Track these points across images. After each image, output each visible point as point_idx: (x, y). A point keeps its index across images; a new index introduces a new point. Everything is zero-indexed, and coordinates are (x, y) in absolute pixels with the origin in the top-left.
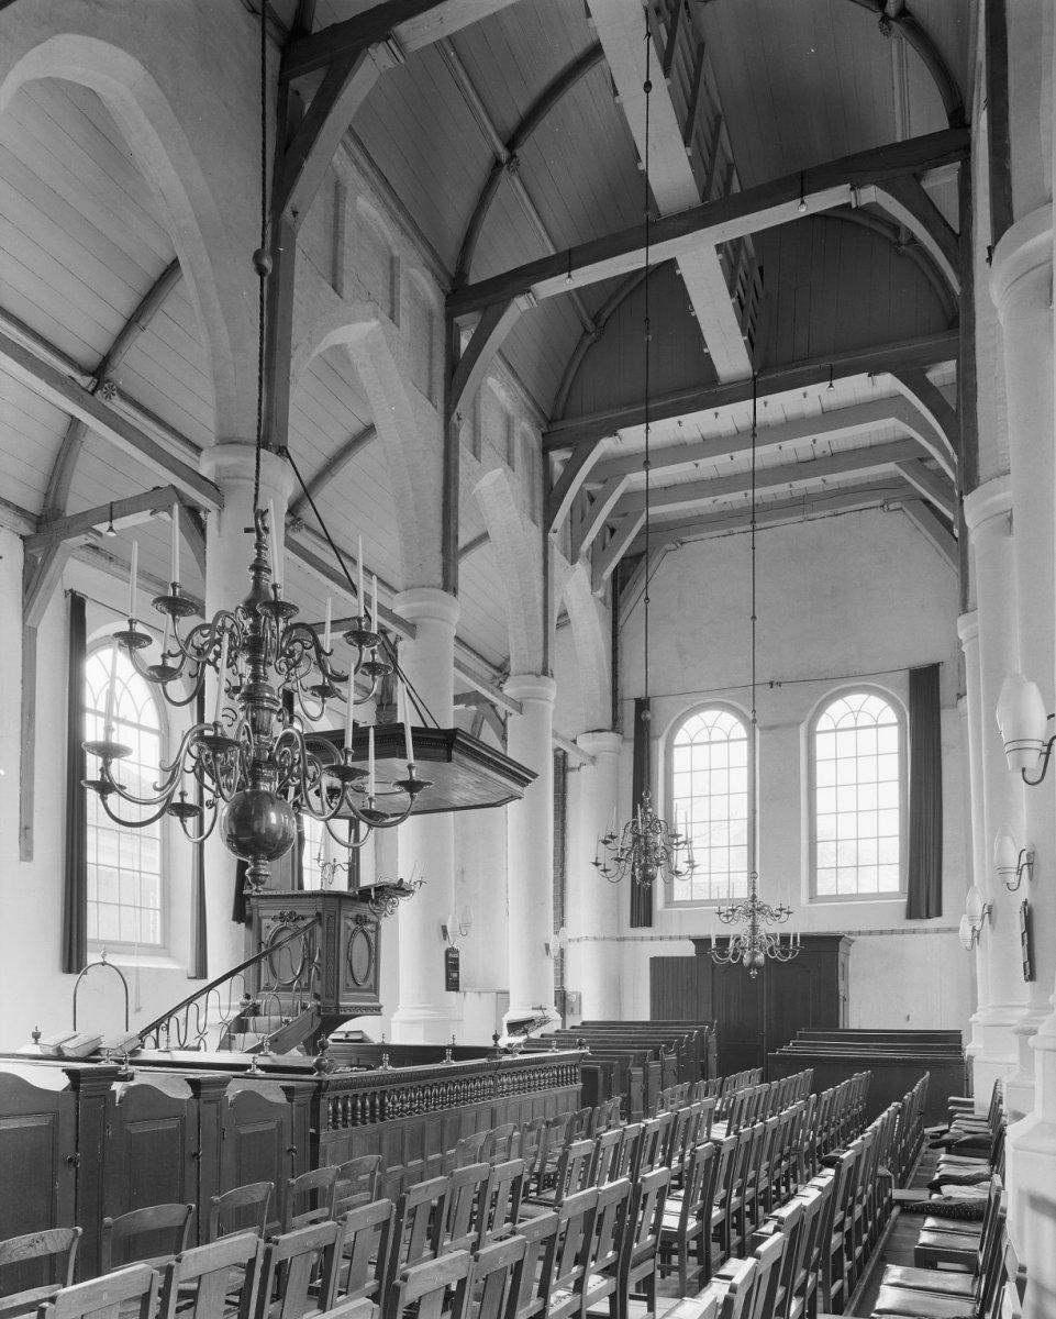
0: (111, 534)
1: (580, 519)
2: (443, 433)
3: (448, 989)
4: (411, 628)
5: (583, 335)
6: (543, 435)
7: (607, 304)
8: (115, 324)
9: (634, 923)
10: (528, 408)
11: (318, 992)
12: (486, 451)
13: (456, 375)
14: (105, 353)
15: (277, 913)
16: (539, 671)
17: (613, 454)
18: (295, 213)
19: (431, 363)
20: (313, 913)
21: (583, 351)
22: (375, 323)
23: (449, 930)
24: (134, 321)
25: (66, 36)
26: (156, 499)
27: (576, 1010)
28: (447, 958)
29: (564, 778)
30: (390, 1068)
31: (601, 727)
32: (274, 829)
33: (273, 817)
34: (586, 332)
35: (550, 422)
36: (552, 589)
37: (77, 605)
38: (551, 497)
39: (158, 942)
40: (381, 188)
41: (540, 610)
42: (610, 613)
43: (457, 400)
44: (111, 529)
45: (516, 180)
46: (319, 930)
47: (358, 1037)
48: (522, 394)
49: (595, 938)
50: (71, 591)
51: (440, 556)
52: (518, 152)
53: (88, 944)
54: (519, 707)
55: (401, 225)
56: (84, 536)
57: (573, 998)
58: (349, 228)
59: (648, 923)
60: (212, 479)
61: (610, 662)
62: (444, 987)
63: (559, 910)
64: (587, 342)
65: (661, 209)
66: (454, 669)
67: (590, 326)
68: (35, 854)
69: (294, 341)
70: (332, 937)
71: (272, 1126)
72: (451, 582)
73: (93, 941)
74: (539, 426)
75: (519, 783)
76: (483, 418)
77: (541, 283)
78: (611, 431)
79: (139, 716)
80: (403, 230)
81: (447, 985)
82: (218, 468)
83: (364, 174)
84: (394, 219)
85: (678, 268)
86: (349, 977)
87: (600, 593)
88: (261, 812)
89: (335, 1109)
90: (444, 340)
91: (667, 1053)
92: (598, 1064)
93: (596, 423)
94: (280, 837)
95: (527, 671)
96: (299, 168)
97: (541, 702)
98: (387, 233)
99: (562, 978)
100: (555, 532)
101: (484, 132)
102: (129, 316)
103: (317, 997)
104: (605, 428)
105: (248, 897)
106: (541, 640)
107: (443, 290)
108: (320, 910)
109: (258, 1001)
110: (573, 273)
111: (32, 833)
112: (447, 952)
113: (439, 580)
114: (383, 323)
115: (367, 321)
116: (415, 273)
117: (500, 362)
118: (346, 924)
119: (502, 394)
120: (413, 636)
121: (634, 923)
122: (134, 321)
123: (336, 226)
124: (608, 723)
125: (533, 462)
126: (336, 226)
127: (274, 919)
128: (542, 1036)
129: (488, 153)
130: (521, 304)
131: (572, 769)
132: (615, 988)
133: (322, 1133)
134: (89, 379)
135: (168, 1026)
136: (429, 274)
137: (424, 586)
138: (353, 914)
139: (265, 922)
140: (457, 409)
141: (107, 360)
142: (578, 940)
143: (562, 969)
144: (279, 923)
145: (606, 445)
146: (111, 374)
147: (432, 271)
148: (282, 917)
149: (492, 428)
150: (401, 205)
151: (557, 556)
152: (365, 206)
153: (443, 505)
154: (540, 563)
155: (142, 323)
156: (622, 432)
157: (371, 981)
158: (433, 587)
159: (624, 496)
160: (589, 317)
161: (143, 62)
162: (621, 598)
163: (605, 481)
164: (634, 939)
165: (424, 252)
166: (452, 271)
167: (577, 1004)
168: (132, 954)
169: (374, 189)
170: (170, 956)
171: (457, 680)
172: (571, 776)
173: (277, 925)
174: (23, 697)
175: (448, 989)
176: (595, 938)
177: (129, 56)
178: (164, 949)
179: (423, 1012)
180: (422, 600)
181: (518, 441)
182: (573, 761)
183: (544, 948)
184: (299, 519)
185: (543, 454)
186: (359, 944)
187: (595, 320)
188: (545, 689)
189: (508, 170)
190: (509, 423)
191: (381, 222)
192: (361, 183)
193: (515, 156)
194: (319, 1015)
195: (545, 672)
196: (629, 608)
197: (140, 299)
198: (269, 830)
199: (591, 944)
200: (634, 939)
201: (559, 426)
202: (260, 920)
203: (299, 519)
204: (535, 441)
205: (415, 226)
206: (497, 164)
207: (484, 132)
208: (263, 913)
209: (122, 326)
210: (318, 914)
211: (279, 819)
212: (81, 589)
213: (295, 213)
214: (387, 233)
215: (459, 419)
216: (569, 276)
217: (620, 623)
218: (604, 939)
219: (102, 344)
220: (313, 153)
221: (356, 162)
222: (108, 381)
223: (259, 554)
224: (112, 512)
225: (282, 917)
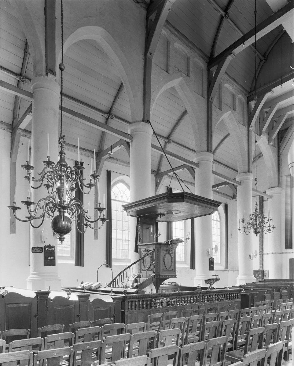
0: (112, 154)
1: (262, 120)
2: (207, 105)
3: (210, 270)
4: (197, 165)
5: (260, 61)
6: (247, 97)
7: (267, 50)
8: (112, 99)
9: (286, 248)
10: (241, 90)
11: (154, 271)
12: (224, 107)
13: (211, 86)
14: (110, 107)
15: (145, 250)
16: (247, 171)
17: (278, 96)
18: (151, 54)
19: (202, 85)
20: (153, 249)
21: (260, 67)
22: (181, 78)
23: (209, 252)
24: (116, 97)
25: (82, 28)
26: (120, 142)
27: (267, 276)
28: (210, 261)
29: (263, 204)
30: (180, 292)
31: (274, 186)
32: (64, 225)
33: (64, 223)
34: (261, 61)
35: (249, 93)
36: (251, 145)
37: (109, 173)
38: (250, 115)
39: (184, 260)
40: (182, 38)
41: (247, 152)
42: (276, 149)
43: (211, 94)
44: (111, 152)
45: (229, 20)
46: (154, 253)
47: (174, 284)
48: (238, 87)
49: (273, 253)
50: (107, 170)
51: (206, 142)
52: (228, 11)
53: (113, 260)
54: (240, 183)
55: (190, 47)
56: (106, 155)
57: (265, 272)
58: (171, 53)
59: (291, 247)
60: (130, 134)
61: (277, 165)
62: (209, 269)
63: (262, 245)
64: (262, 63)
65: (273, 10)
66: (212, 174)
67: (262, 58)
68: (98, 238)
69: (152, 90)
70: (158, 256)
71: (107, 308)
72: (210, 149)
73: (114, 259)
74: (246, 95)
75: (214, 206)
76: (222, 97)
77: (235, 49)
78: (269, 90)
79: (116, 198)
80: (191, 48)
81: (52, 265)
82: (131, 130)
83: (176, 36)
84: (188, 46)
85: (284, 28)
86: (164, 266)
87: (272, 143)
88: (59, 221)
89: (132, 305)
90: (207, 77)
91: (283, 289)
92: (248, 293)
93: (264, 89)
94: (66, 227)
95: (243, 172)
96: (151, 40)
97: (247, 181)
98: (186, 51)
99: (262, 266)
100: (252, 127)
101: (216, 10)
102: (115, 96)
103: (154, 272)
104: (268, 90)
105: (138, 245)
106: (247, 162)
107: (206, 62)
108: (155, 248)
109: (141, 274)
110: (245, 43)
111: (98, 232)
112: (210, 259)
113: (206, 149)
114: (184, 77)
115: (178, 78)
116: (196, 60)
117: (229, 79)
118: (162, 253)
119: (231, 88)
120: (198, 167)
121: (286, 248)
122: (116, 97)
123: (167, 54)
124: (276, 185)
125: (244, 107)
126: (167, 54)
127: (144, 251)
128: (247, 284)
129: (219, 15)
130: (230, 58)
131: (265, 201)
132: (279, 268)
133: (126, 311)
134: (107, 115)
135: (115, 281)
136: (201, 58)
137: (201, 152)
138: (165, 249)
139: (142, 252)
140: (211, 96)
141: (111, 109)
142: (268, 254)
143: (262, 263)
144: (145, 252)
145: (268, 95)
146: (112, 112)
147: (202, 57)
148: (146, 251)
149: (227, 99)
150: (189, 41)
151: (253, 134)
152: (178, 45)
153: (207, 126)
154: (247, 138)
155: (118, 97)
156: (273, 89)
157: (172, 267)
158: (204, 151)
159: (276, 112)
160: (262, 55)
161: (103, 28)
162: (281, 144)
163: (270, 107)
164: (286, 253)
165: (199, 52)
166: (209, 55)
167: (267, 274)
168: (125, 262)
169: (180, 39)
170: (186, 264)
171: (215, 178)
172: (265, 203)
173: (145, 253)
174: (95, 198)
175: (210, 270)
176: (273, 253)
177: (100, 27)
178: (185, 262)
179: (202, 277)
180: (200, 156)
181: (237, 102)
182: (265, 198)
183: (249, 256)
184: (170, 140)
185: (247, 103)
186: (168, 257)
187: (264, 56)
188: (248, 177)
189: (226, 18)
190: (234, 97)
191: (183, 48)
192: (175, 39)
193: (227, 13)
194: (154, 278)
195: (248, 172)
196: (284, 145)
197: (117, 91)
198: (62, 226)
199: (271, 255)
200: (286, 253)
201: (252, 93)
202: (141, 251)
203: (170, 140)
204: (244, 100)
205: (195, 46)
206: (222, 18)
207: (216, 10)
208: (142, 250)
209: (114, 99)
210: (154, 249)
211: (65, 223)
212: (109, 169)
213: (151, 54)
214: (186, 51)
215: (212, 99)
216: (244, 44)
217: (281, 152)
218: (276, 253)
219: (109, 105)
220: (154, 35)
221: (173, 33)
222: (111, 114)
223: (62, 149)
224: (112, 148)
225: (146, 251)
